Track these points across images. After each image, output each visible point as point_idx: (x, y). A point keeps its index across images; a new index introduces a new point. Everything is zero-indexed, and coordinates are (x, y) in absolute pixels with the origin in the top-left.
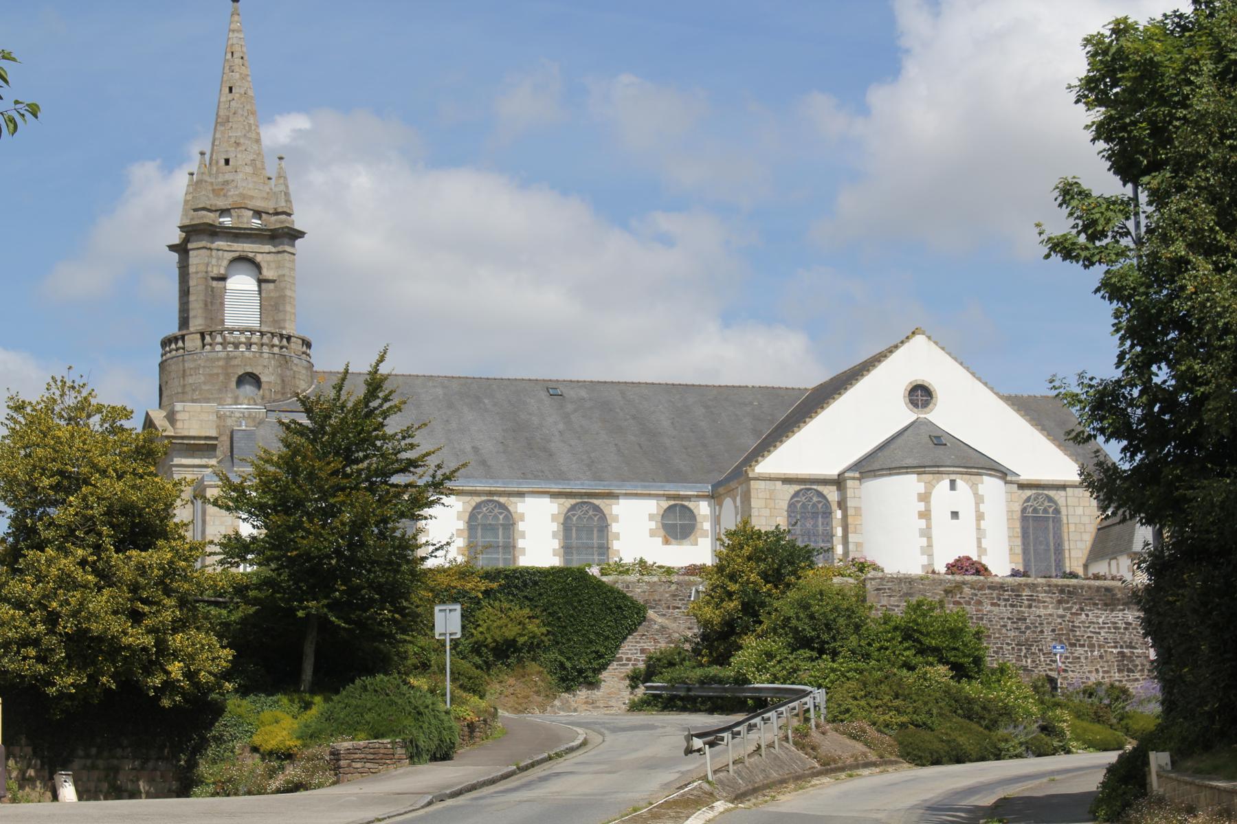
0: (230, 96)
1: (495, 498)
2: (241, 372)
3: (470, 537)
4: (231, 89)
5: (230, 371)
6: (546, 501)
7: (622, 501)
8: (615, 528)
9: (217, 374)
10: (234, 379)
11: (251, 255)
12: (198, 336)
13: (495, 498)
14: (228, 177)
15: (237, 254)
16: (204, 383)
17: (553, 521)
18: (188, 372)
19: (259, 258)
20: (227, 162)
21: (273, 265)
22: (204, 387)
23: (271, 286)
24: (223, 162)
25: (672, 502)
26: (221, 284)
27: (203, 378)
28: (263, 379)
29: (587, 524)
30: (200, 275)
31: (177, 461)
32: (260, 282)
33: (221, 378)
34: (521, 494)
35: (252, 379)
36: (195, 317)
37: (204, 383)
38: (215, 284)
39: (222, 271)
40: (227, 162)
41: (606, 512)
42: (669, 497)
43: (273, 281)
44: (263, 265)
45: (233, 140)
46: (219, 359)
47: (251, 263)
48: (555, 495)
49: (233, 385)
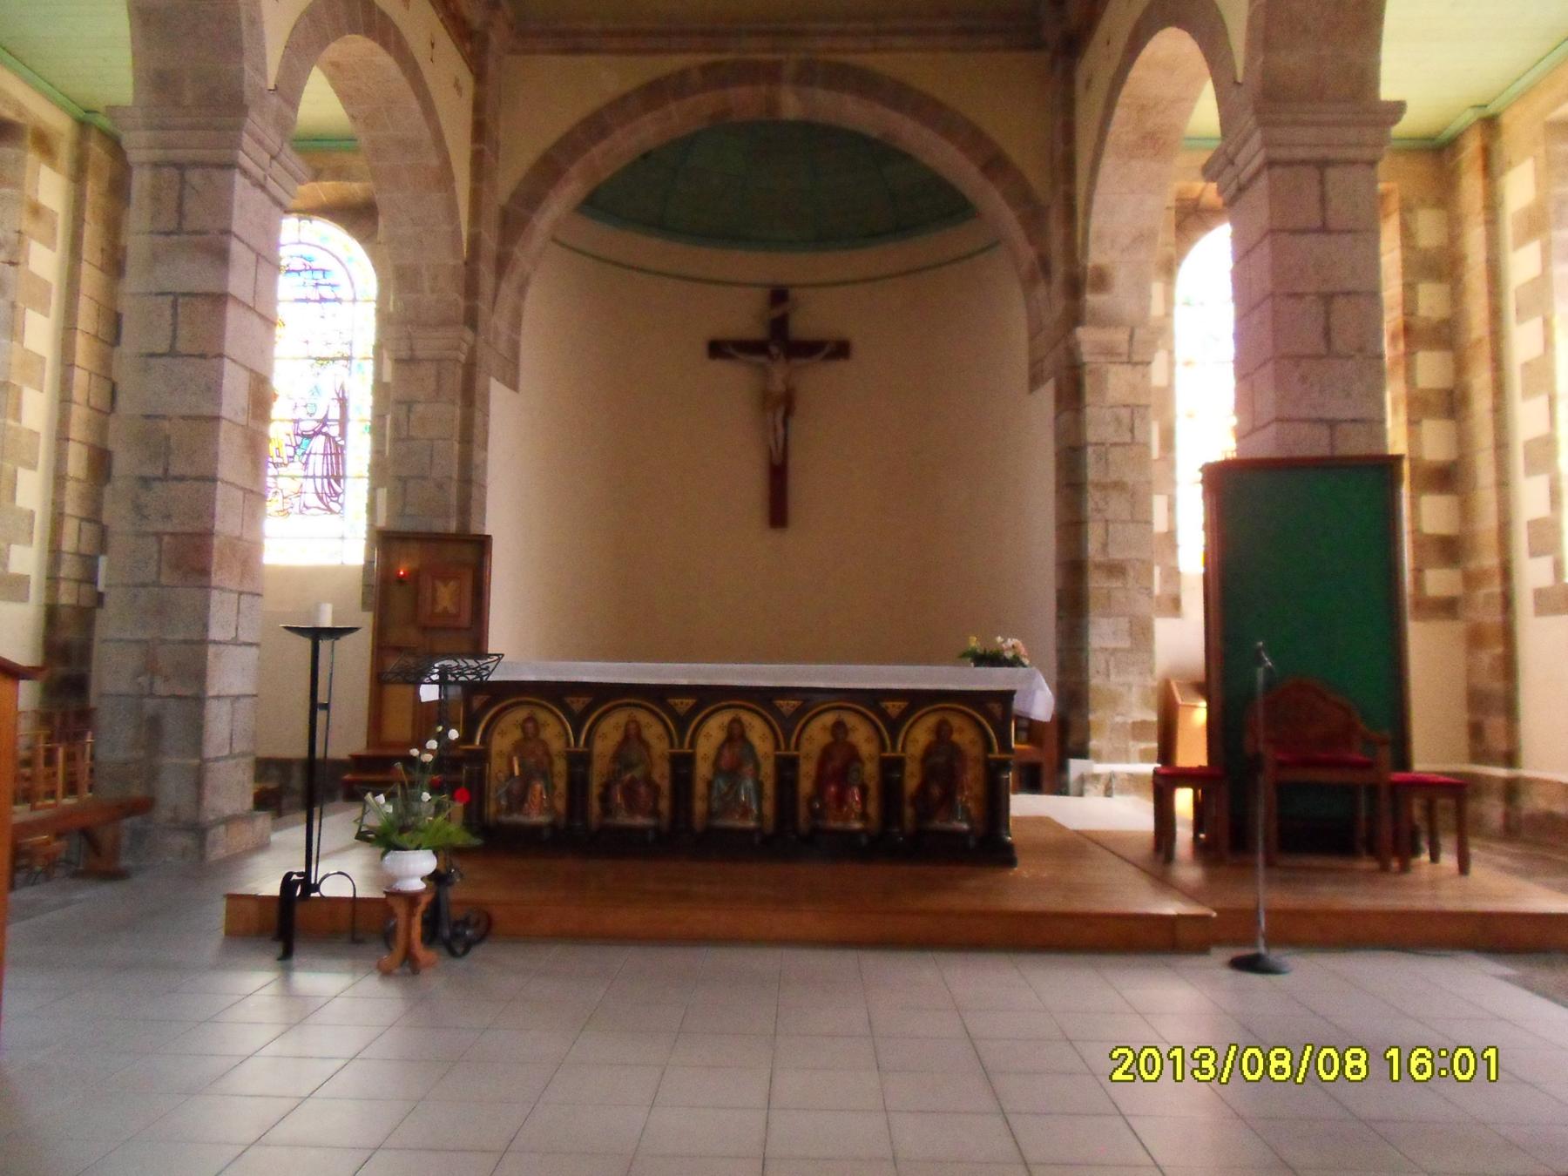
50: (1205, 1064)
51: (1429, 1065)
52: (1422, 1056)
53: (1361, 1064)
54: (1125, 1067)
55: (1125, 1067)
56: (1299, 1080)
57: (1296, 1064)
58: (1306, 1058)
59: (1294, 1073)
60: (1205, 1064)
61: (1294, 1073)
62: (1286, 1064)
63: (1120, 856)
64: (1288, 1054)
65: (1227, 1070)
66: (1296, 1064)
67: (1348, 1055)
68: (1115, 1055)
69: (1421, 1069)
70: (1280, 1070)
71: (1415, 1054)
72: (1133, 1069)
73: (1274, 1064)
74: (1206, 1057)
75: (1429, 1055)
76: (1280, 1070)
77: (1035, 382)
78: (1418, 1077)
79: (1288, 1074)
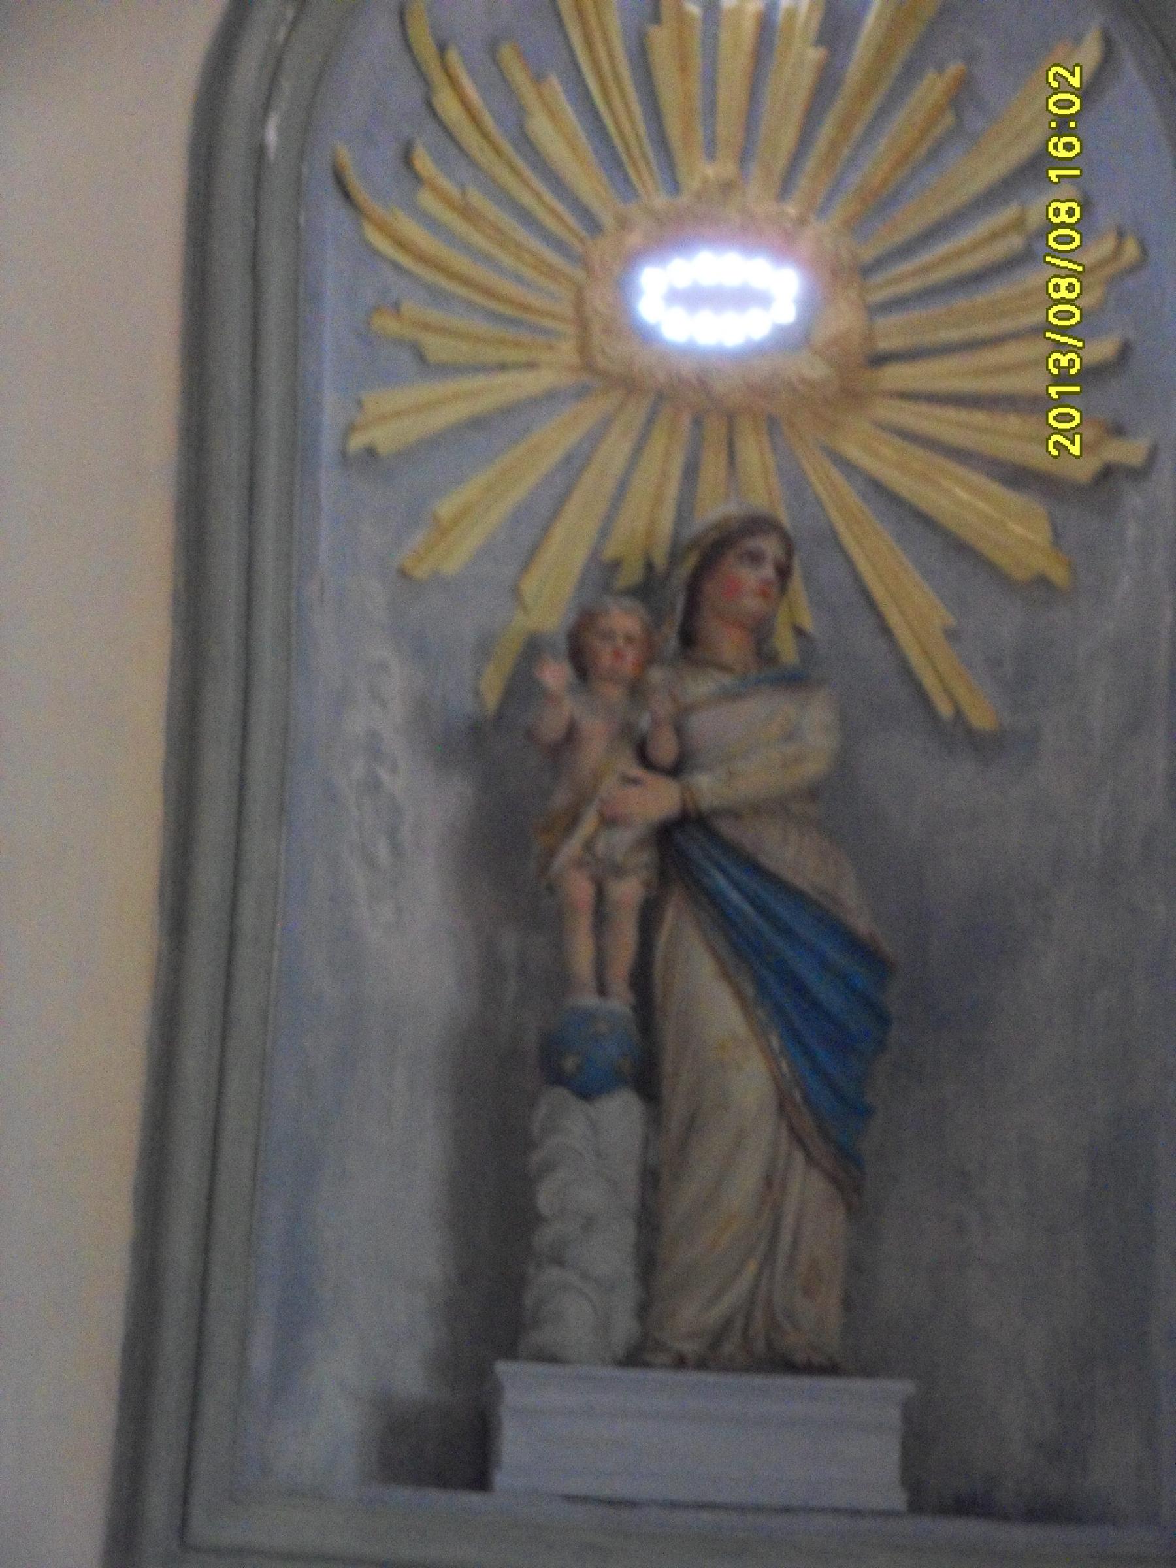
50: (1064, 363)
51: (1065, 139)
52: (1056, 146)
53: (1064, 207)
54: (1066, 74)
55: (1066, 74)
56: (1080, 344)
57: (1066, 272)
58: (1058, 262)
59: (1074, 274)
60: (1064, 363)
61: (1074, 274)
62: (1064, 283)
63: (224, 1038)
64: (1054, 281)
65: (1070, 266)
66: (1066, 272)
67: (1055, 296)
68: (1055, 84)
69: (1069, 147)
70: (1070, 288)
71: (1054, 153)
72: (1069, 435)
73: (1064, 293)
74: (1057, 361)
75: (1055, 139)
76: (1070, 288)
77: (538, 79)
78: (1077, 150)
79: (1074, 280)
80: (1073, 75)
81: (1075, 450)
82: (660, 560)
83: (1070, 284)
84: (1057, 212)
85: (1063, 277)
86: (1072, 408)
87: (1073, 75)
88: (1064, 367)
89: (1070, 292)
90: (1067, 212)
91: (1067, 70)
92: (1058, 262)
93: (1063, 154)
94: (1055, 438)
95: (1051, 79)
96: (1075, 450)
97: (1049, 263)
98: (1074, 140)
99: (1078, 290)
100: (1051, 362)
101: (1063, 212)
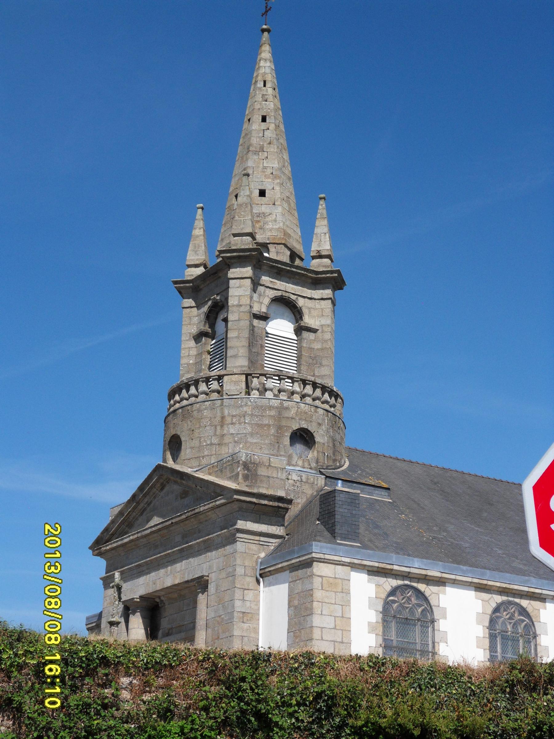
0: (264, 125)
1: (517, 600)
2: (295, 427)
3: (384, 633)
4: (264, 119)
5: (284, 423)
6: (471, 594)
7: (450, 590)
8: (442, 625)
9: (269, 426)
10: (288, 434)
11: (293, 297)
12: (243, 378)
13: (517, 600)
14: (264, 209)
15: (279, 293)
16: (252, 434)
17: (479, 623)
18: (228, 420)
19: (301, 302)
20: (262, 193)
21: (314, 313)
22: (250, 440)
23: (312, 336)
24: (257, 192)
25: (400, 582)
26: (261, 324)
27: (249, 429)
28: (318, 439)
29: (407, 613)
30: (242, 309)
31: (241, 524)
32: (299, 330)
33: (273, 431)
34: (441, 582)
35: (303, 437)
36: (235, 356)
37: (252, 434)
38: (256, 322)
39: (264, 310)
40: (262, 193)
41: (433, 602)
42: (502, 591)
43: (315, 331)
44: (305, 310)
45: (269, 171)
46: (271, 408)
47: (288, 306)
48: (480, 588)
49: (287, 441)
50: (53, 568)
52: (57, 670)
54: (52, 530)
55: (52, 530)
60: (53, 568)
62: (53, 606)
66: (52, 611)
69: (51, 670)
71: (57, 667)
72: (50, 534)
74: (56, 569)
75: (57, 673)
80: (49, 530)
81: (47, 527)
82: (288, 571)
83: (50, 605)
84: (56, 603)
85: (53, 608)
86: (49, 547)
87: (49, 530)
88: (53, 566)
89: (50, 601)
90: (51, 639)
91: (51, 532)
92: (56, 580)
93: (53, 666)
94: (57, 533)
95: (59, 528)
96: (47, 527)
97: (60, 615)
98: (48, 673)
99: (46, 602)
100: (59, 569)
101: (53, 639)
